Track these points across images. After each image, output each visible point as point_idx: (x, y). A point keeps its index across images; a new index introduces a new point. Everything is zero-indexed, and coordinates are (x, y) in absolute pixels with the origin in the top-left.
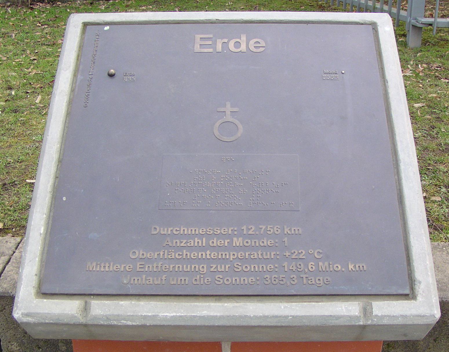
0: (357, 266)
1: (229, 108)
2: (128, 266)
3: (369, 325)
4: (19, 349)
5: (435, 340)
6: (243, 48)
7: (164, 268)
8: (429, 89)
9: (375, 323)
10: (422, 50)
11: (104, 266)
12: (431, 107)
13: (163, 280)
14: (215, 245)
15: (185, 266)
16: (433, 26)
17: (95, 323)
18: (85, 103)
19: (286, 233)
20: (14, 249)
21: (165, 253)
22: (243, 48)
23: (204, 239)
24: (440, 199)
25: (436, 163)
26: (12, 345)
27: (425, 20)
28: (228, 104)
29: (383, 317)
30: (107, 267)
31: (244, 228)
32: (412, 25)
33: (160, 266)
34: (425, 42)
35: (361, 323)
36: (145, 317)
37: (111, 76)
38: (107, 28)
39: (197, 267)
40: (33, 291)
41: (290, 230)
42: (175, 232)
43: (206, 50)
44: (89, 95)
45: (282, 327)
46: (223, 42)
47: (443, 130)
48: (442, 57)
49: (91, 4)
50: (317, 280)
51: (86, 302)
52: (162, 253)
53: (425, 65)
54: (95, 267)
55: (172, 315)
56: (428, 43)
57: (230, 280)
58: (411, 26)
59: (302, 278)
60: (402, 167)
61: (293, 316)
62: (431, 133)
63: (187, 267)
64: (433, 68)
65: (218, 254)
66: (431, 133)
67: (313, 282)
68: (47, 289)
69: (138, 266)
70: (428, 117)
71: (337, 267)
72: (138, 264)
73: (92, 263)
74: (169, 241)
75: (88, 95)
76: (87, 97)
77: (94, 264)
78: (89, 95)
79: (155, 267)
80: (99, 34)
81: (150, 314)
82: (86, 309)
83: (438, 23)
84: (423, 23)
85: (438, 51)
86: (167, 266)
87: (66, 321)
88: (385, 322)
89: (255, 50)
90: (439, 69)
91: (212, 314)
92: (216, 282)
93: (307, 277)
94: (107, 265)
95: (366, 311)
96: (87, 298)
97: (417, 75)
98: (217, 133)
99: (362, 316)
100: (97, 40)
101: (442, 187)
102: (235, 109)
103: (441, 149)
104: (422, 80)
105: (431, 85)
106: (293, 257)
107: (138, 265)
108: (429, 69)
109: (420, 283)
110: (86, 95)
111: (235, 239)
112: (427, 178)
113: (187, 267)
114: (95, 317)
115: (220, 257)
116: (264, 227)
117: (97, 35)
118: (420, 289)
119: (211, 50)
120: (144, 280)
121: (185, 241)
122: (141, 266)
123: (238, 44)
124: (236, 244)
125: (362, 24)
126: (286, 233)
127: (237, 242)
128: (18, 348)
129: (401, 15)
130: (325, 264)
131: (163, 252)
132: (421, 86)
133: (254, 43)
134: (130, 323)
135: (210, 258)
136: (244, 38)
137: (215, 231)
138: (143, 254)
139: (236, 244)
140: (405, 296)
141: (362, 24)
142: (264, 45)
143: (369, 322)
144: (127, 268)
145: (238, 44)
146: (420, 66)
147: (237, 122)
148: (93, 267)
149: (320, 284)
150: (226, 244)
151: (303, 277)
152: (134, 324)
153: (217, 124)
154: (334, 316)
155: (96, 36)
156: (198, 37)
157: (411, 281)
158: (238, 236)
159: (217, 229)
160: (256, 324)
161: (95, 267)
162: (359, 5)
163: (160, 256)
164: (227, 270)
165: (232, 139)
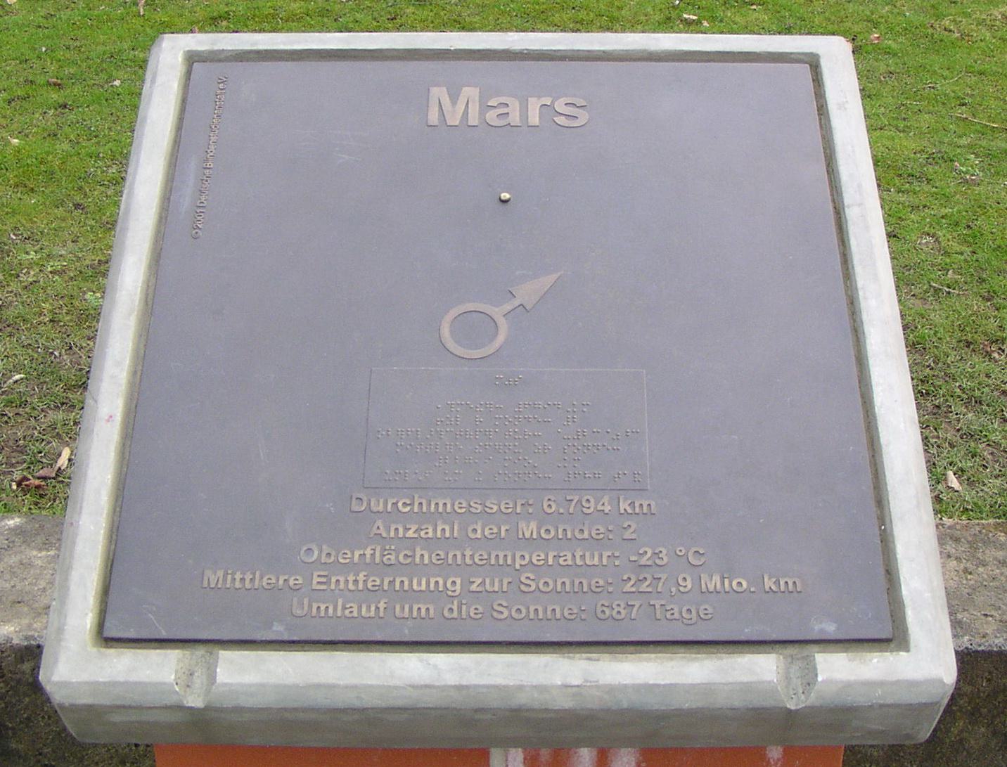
0: (782, 583)
2: (293, 578)
7: (370, 585)
11: (241, 579)
13: (382, 610)
14: (479, 535)
15: (415, 581)
18: (195, 229)
19: (622, 511)
21: (375, 553)
30: (247, 582)
33: (361, 577)
39: (441, 582)
44: (203, 212)
46: (501, 104)
50: (684, 610)
52: (368, 552)
54: (221, 581)
57: (524, 611)
59: (653, 607)
63: (419, 584)
65: (489, 555)
67: (677, 616)
68: (107, 634)
69: (316, 579)
71: (740, 583)
72: (315, 574)
73: (215, 573)
74: (381, 527)
75: (201, 212)
76: (199, 216)
77: (220, 573)
78: (203, 212)
79: (238, 580)
80: (225, 79)
86: (272, 578)
92: (495, 614)
93: (664, 605)
100: (219, 92)
107: (315, 576)
110: (198, 211)
113: (419, 584)
115: (493, 562)
117: (219, 81)
120: (340, 608)
121: (414, 528)
122: (324, 580)
124: (523, 534)
126: (622, 511)
127: (480, 530)
130: (714, 578)
131: (372, 549)
133: (497, 116)
135: (471, 562)
137: (584, 507)
138: (329, 554)
139: (523, 534)
144: (291, 582)
148: (218, 581)
149: (691, 619)
150: (503, 534)
151: (654, 605)
155: (219, 83)
159: (476, 503)
161: (221, 581)
163: (365, 559)
164: (505, 590)
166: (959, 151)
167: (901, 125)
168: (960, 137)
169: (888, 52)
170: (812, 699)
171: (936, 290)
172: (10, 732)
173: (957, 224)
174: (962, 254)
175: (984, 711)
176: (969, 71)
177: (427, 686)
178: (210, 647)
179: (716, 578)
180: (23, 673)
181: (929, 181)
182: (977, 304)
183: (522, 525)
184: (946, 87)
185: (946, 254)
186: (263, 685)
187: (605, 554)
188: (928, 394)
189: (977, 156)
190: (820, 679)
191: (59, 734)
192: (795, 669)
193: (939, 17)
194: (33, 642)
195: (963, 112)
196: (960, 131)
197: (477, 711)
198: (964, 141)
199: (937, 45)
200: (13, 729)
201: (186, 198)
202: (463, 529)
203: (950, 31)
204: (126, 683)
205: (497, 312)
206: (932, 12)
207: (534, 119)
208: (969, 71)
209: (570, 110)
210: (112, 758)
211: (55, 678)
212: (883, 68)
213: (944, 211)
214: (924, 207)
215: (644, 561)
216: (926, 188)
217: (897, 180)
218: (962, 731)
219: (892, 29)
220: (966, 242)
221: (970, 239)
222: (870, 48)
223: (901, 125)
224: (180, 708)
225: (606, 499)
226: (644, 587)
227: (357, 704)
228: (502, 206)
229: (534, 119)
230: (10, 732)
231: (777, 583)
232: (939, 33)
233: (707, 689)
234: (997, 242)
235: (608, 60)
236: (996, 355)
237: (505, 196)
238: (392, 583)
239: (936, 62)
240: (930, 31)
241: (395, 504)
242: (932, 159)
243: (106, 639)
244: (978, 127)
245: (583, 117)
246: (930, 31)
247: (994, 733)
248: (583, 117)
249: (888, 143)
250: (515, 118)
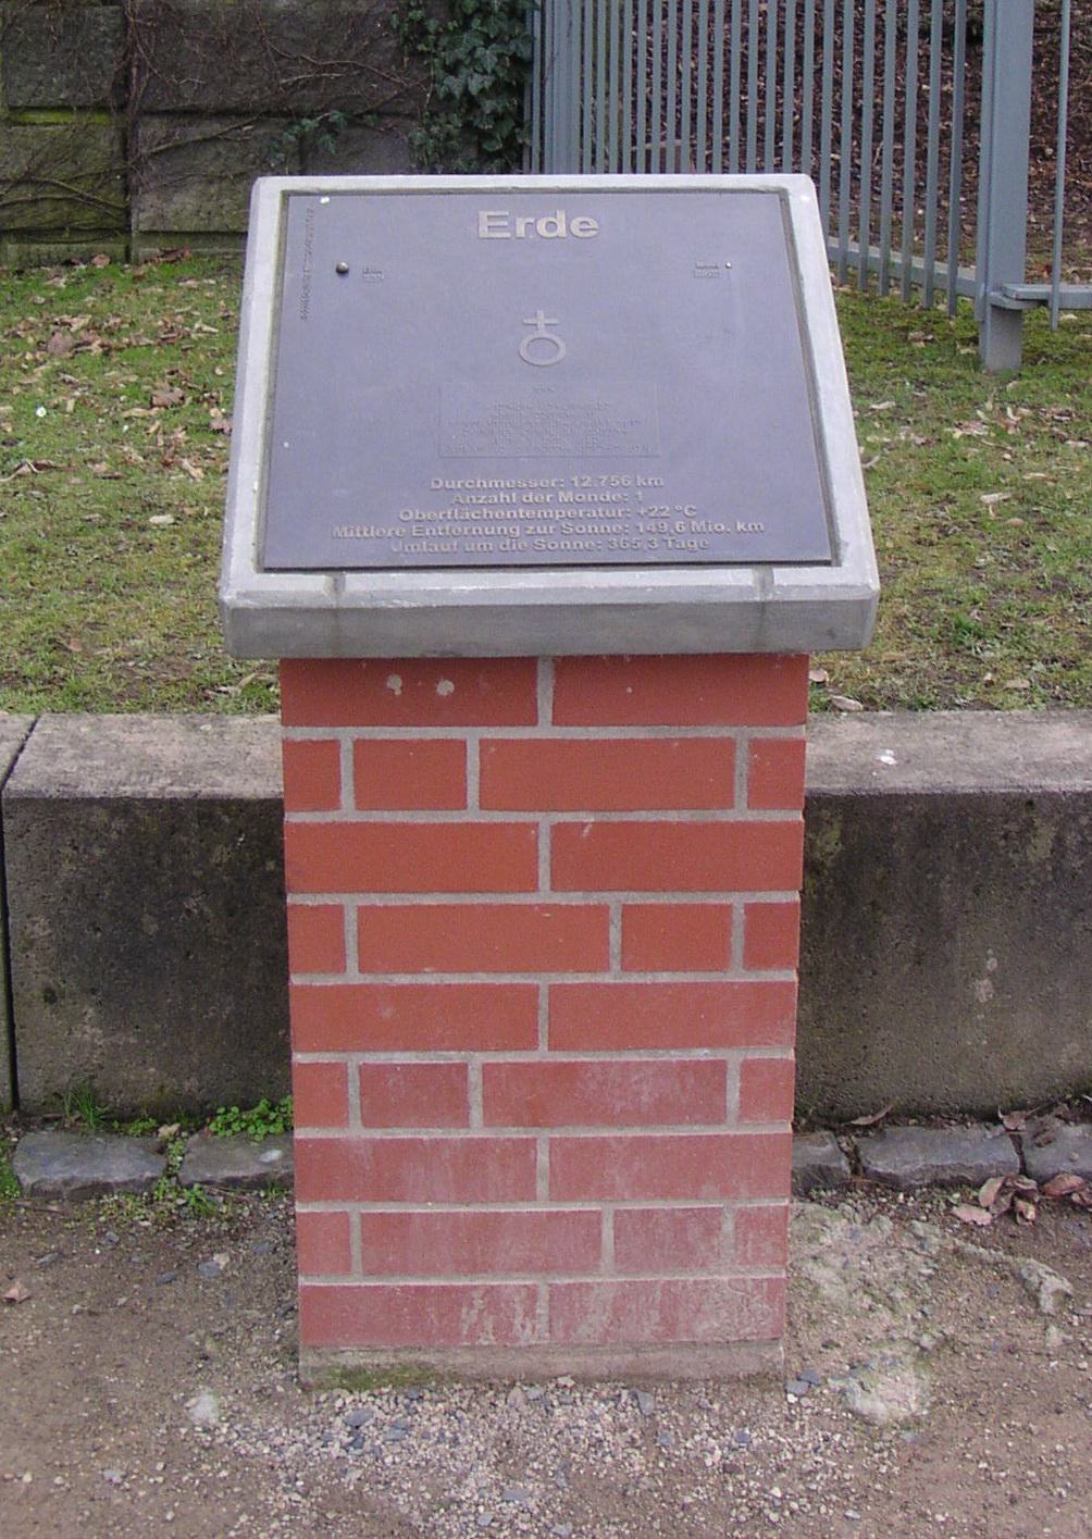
1: (542, 320)
3: (770, 603)
4: (50, 935)
5: (977, 891)
6: (561, 230)
8: (1028, 463)
9: (776, 598)
10: (1023, 373)
12: (1028, 501)
16: (1050, 304)
17: (353, 606)
20: (25, 730)
22: (561, 230)
23: (514, 495)
24: (1026, 684)
25: (1025, 616)
26: (34, 923)
27: (1027, 290)
28: (541, 314)
29: (791, 588)
31: (575, 479)
32: (993, 306)
34: (1033, 357)
35: (757, 599)
36: (430, 593)
37: (342, 272)
38: (325, 200)
40: (251, 565)
41: (646, 481)
42: (467, 485)
43: (499, 235)
45: (636, 607)
47: (1051, 548)
48: (1076, 389)
49: (20, 272)
51: (335, 580)
53: (1025, 411)
55: (471, 588)
56: (1044, 359)
58: (989, 309)
60: (822, 396)
61: (654, 588)
62: (1021, 554)
64: (1048, 416)
66: (1021, 554)
68: (270, 562)
70: (1016, 520)
77: (345, 529)
81: (438, 588)
82: (337, 588)
83: (1062, 297)
84: (1022, 297)
85: (1068, 376)
87: (306, 604)
88: (794, 596)
89: (581, 234)
90: (1064, 418)
91: (533, 586)
94: (366, 530)
95: (765, 584)
96: (337, 575)
97: (1001, 433)
98: (523, 353)
99: (759, 588)
101: (1035, 662)
102: (553, 321)
103: (1042, 586)
104: (1013, 444)
105: (1034, 454)
106: (652, 514)
108: (1037, 420)
109: (847, 544)
111: (561, 494)
112: (998, 645)
114: (353, 596)
116: (605, 478)
118: (847, 554)
119: (508, 235)
123: (552, 226)
125: (762, 192)
128: (48, 931)
129: (962, 280)
132: (1007, 456)
134: (406, 604)
136: (561, 216)
140: (827, 563)
141: (762, 192)
142: (596, 226)
143: (770, 597)
145: (552, 226)
146: (1009, 411)
147: (556, 339)
152: (413, 605)
153: (525, 342)
154: (716, 587)
156: (484, 215)
157: (835, 544)
158: (565, 490)
160: (598, 602)
162: (845, 259)
165: (553, 360)
178: (767, 567)
238: (470, 531)
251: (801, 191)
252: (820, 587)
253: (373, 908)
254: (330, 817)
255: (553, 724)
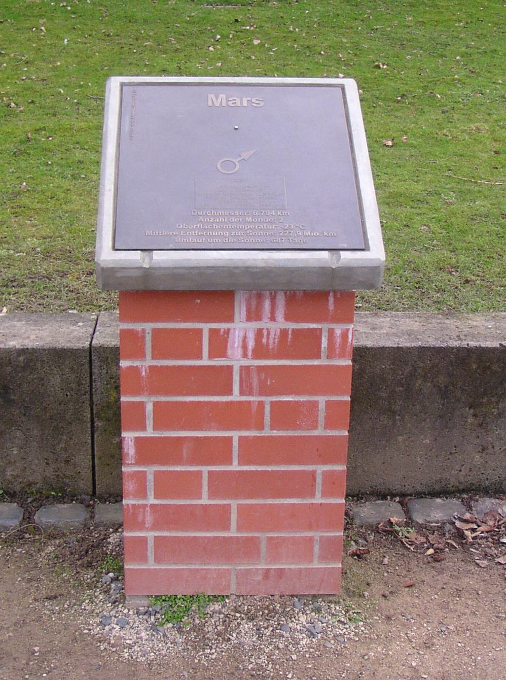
33: (197, 232)
68: (116, 248)
166: (444, 190)
167: (415, 179)
168: (447, 184)
169: (412, 146)
170: (340, 264)
171: (427, 248)
172: (11, 391)
173: (440, 221)
174: (441, 233)
175: (429, 375)
176: (455, 154)
177: (219, 259)
178: (149, 251)
179: (309, 232)
180: (20, 362)
181: (427, 203)
182: (446, 253)
183: (247, 218)
184: (442, 162)
185: (433, 233)
186: (167, 260)
187: (274, 226)
188: (419, 288)
189: (454, 192)
190: (342, 258)
191: (33, 391)
192: (334, 257)
193: (441, 129)
194: (25, 347)
195: (450, 173)
196: (447, 182)
197: (235, 268)
198: (448, 186)
199: (439, 142)
200: (12, 389)
201: (126, 128)
202: (228, 220)
203: (446, 136)
204: (124, 260)
205: (236, 161)
206: (438, 127)
207: (245, 104)
208: (455, 154)
209: (257, 102)
210: (56, 402)
211: (101, 259)
212: (408, 153)
213: (434, 216)
214: (424, 214)
215: (286, 228)
216: (425, 206)
217: (411, 203)
218: (420, 385)
219: (414, 135)
220: (444, 228)
221: (446, 227)
222: (401, 144)
223: (415, 179)
224: (142, 268)
225: (273, 211)
226: (286, 235)
227: (198, 265)
228: (235, 131)
229: (245, 104)
230: (11, 391)
231: (328, 234)
232: (440, 136)
233: (307, 260)
234: (460, 228)
235: (271, 86)
236: (454, 273)
237: (236, 127)
238: (206, 233)
239: (437, 150)
240: (436, 136)
241: (206, 213)
242: (430, 193)
243: (115, 249)
244: (457, 180)
245: (262, 104)
246: (436, 136)
247: (434, 386)
248: (262, 104)
249: (407, 187)
250: (238, 104)
251: (351, 86)
252: (254, 260)
253: (247, 437)
254: (275, 399)
255: (247, 320)
